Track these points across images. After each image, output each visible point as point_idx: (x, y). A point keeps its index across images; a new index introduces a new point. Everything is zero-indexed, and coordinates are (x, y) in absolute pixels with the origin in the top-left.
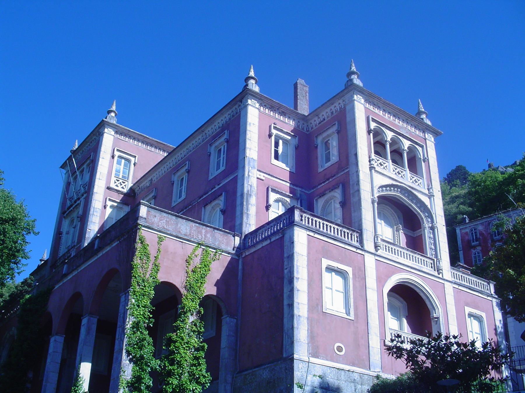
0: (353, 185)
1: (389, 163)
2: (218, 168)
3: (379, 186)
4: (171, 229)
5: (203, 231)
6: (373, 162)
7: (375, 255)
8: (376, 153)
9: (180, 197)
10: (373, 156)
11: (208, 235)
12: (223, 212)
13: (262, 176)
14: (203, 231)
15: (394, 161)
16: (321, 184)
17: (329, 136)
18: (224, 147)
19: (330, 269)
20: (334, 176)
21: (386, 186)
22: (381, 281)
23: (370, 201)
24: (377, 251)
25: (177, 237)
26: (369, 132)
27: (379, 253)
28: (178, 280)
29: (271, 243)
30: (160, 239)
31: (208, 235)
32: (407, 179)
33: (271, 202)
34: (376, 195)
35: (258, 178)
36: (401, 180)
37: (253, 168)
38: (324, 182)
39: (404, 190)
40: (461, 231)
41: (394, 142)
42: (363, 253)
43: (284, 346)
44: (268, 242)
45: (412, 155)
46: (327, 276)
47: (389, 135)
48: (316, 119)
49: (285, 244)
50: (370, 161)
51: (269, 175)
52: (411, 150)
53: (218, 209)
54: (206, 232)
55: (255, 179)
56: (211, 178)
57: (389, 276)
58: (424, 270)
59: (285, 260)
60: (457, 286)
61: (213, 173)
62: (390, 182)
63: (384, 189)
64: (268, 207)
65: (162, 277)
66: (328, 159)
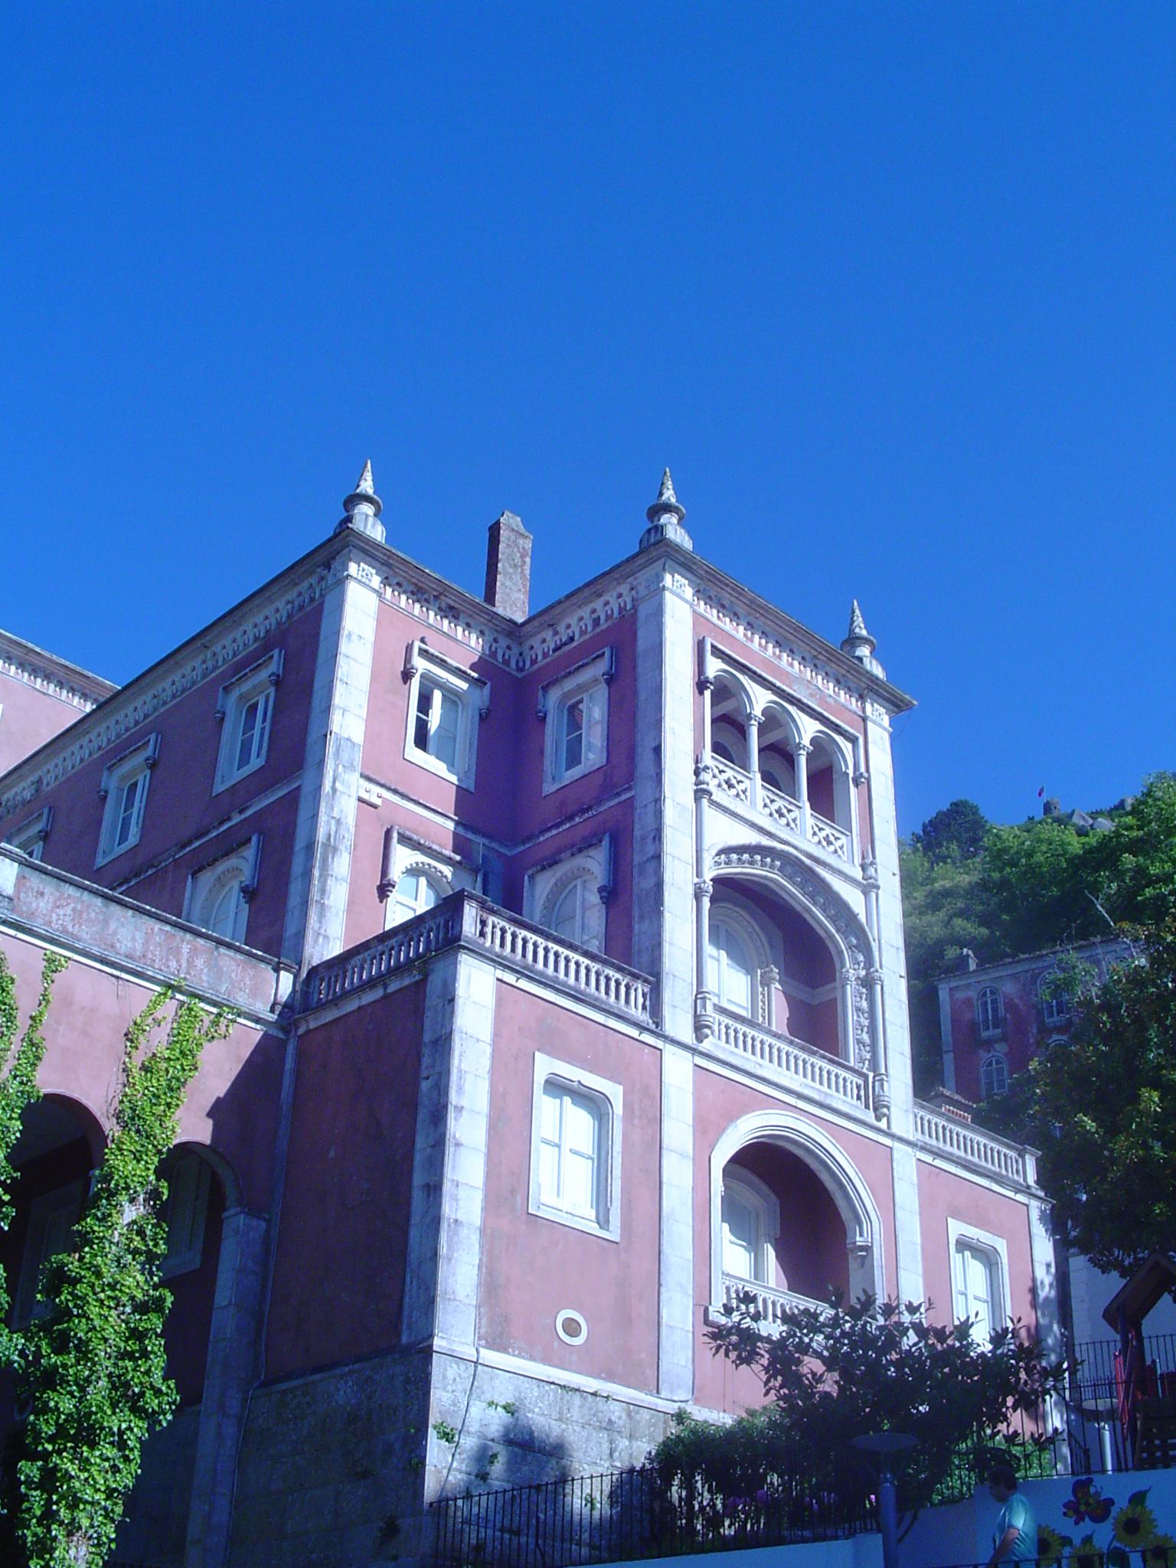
0: (643, 839)
1: (755, 783)
2: (244, 760)
3: (720, 847)
4: (86, 935)
5: (185, 949)
6: (705, 776)
7: (694, 1051)
8: (718, 749)
9: (123, 839)
10: (708, 757)
11: (199, 962)
12: (249, 893)
13: (374, 794)
14: (185, 949)
15: (768, 778)
16: (549, 829)
17: (581, 688)
18: (266, 699)
19: (556, 1087)
20: (590, 808)
21: (740, 850)
22: (706, 1131)
23: (691, 890)
24: (700, 1040)
25: (103, 961)
26: (701, 685)
27: (706, 1045)
28: (98, 1094)
29: (386, 997)
30: (52, 965)
31: (199, 962)
32: (802, 830)
33: (396, 873)
34: (709, 873)
35: (360, 800)
36: (784, 834)
37: (350, 767)
38: (557, 826)
39: (792, 865)
40: (951, 996)
41: (772, 720)
42: (659, 1044)
43: (406, 1312)
44: (378, 993)
45: (821, 763)
46: (546, 1107)
47: (760, 699)
48: (548, 634)
49: (427, 1004)
50: (697, 773)
51: (395, 792)
52: (821, 748)
53: (235, 885)
54: (194, 952)
55: (354, 803)
56: (219, 787)
57: (731, 1117)
58: (835, 1104)
59: (426, 1051)
60: (928, 1158)
61: (229, 774)
62: (753, 838)
63: (734, 856)
64: (384, 890)
65: (47, 1081)
66: (574, 759)
